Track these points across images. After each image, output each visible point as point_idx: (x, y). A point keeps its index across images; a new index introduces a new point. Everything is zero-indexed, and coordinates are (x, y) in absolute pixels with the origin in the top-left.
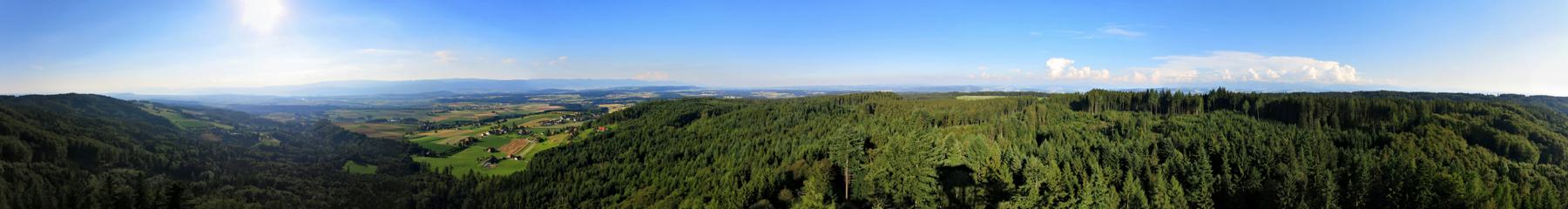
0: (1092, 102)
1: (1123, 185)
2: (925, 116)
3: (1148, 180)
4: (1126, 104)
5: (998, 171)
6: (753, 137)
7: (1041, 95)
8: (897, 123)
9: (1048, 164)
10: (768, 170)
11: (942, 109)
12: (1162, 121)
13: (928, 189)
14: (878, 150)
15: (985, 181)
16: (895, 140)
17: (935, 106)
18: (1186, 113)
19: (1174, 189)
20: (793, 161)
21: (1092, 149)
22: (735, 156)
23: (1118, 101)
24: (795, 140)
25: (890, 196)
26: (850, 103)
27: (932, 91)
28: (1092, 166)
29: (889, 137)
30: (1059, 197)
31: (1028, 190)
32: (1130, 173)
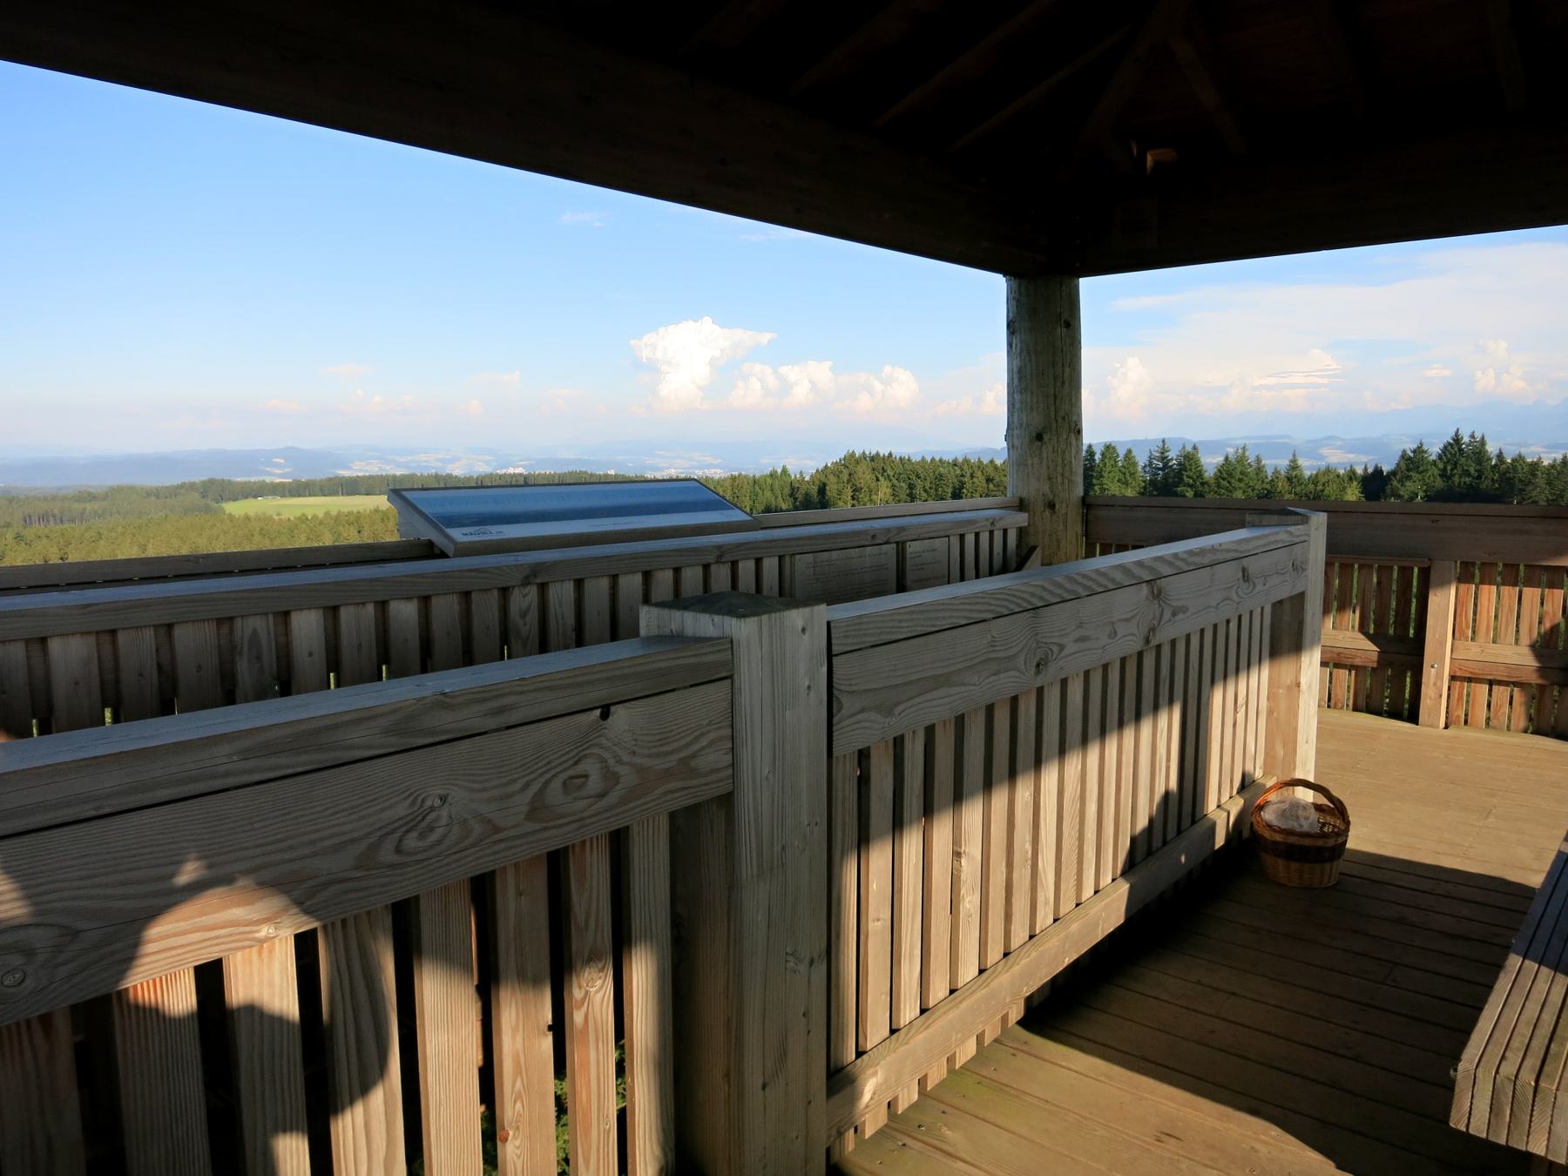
27: (101, 481)
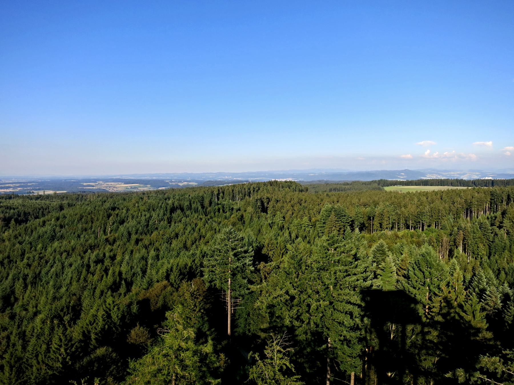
2: (340, 215)
5: (461, 306)
6: (85, 252)
8: (300, 226)
10: (109, 300)
13: (348, 321)
14: (274, 264)
15: (439, 318)
16: (297, 249)
17: (355, 201)
20: (150, 284)
22: (54, 286)
24: (152, 253)
25: (292, 330)
26: (233, 198)
29: (289, 246)
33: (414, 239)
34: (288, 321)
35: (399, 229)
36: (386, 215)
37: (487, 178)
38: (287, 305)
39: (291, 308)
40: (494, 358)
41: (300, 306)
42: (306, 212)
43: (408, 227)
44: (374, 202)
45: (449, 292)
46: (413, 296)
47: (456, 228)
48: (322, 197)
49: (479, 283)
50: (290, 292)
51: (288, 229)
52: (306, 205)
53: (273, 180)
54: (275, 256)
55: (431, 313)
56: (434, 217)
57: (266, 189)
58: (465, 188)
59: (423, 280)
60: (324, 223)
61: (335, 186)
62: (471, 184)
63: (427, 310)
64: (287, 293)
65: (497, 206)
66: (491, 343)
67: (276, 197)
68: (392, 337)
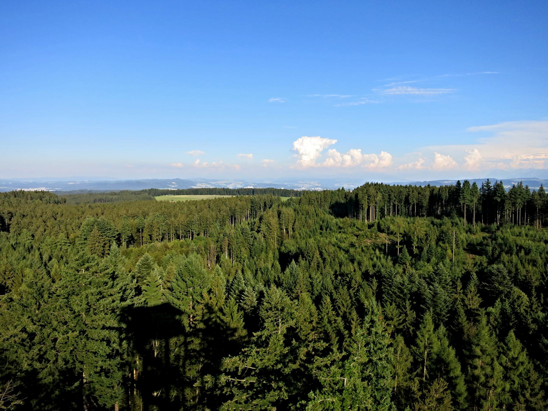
0: (365, 204)
1: (416, 336)
2: (103, 229)
3: (461, 331)
4: (420, 206)
5: (221, 310)
7: (285, 193)
9: (297, 298)
11: (134, 216)
12: (486, 235)
13: (104, 349)
15: (201, 326)
17: (123, 212)
18: (532, 224)
19: (511, 354)
21: (366, 276)
23: (407, 202)
28: (366, 303)
30: (314, 349)
31: (268, 338)
32: (428, 317)
33: (183, 249)
34: (26, 364)
35: (169, 239)
36: (156, 225)
37: (249, 187)
38: (25, 346)
39: (30, 348)
40: (234, 358)
41: (44, 344)
42: (62, 227)
43: (178, 237)
44: (143, 212)
45: (211, 298)
46: (177, 307)
47: (222, 235)
48: (83, 209)
49: (238, 285)
50: (28, 329)
51: (39, 249)
52: (63, 219)
53: (19, 189)
54: (14, 285)
55: (194, 322)
56: (202, 225)
57: (8, 201)
58: (231, 196)
59: (186, 290)
60: (86, 239)
61: (100, 197)
62: (235, 192)
63: (191, 320)
64: (24, 330)
65: (256, 213)
66: (246, 340)
67: (21, 211)
68: (156, 354)
